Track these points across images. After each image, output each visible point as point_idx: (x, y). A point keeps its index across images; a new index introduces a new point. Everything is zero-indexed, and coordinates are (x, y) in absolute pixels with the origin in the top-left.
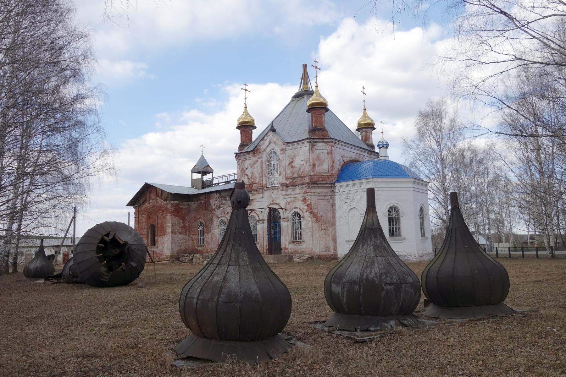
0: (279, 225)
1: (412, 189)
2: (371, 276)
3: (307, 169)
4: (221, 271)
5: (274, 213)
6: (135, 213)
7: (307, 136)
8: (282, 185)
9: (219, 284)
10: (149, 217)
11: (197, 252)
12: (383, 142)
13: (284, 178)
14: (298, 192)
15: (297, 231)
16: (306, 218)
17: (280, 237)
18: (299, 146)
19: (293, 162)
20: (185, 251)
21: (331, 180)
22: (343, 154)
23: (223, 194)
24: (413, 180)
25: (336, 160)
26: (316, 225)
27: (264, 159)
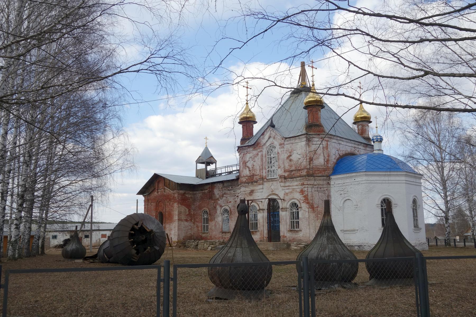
0: (278, 215)
1: (405, 182)
2: (323, 256)
3: (305, 163)
4: (232, 250)
5: (273, 203)
6: (145, 201)
7: (304, 132)
8: (281, 177)
9: (231, 258)
10: (157, 206)
11: (202, 238)
12: (377, 136)
13: (283, 170)
14: (295, 184)
15: (295, 220)
16: (303, 208)
17: (279, 226)
18: (297, 141)
19: (291, 156)
20: (191, 238)
21: (326, 173)
22: (336, 149)
23: (225, 184)
24: (405, 173)
25: (332, 154)
26: (312, 215)
27: (264, 153)
